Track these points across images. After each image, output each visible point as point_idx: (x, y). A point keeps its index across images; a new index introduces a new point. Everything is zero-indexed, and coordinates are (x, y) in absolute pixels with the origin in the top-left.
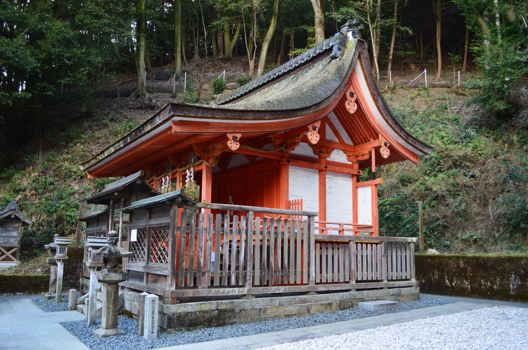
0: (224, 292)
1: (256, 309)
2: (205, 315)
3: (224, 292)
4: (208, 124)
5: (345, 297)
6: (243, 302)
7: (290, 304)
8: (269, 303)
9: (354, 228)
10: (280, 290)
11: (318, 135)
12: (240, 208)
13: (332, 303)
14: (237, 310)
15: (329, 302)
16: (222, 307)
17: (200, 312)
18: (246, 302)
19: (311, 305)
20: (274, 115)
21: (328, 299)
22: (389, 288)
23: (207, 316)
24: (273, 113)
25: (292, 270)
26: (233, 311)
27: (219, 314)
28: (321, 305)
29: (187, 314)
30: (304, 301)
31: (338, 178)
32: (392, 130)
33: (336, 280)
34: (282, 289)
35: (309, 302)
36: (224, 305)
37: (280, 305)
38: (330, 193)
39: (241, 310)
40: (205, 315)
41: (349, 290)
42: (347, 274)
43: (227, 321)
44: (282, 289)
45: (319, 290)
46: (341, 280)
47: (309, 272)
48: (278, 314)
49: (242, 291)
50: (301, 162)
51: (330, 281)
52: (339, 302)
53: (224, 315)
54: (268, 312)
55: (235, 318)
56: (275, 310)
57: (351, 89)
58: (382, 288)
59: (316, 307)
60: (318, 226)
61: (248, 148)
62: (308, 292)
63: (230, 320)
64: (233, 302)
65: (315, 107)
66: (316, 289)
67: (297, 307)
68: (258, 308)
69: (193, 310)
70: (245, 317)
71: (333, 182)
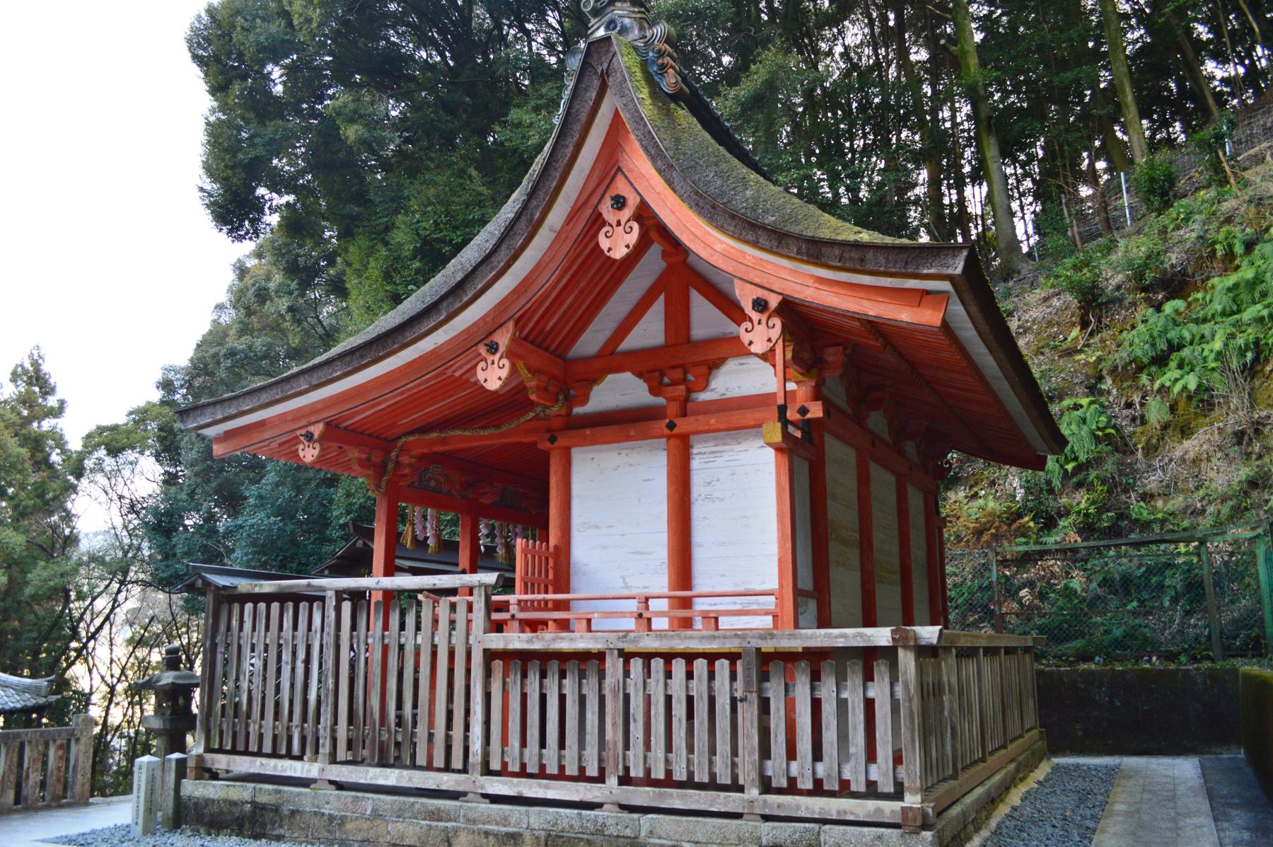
0: (275, 768)
1: (323, 814)
2: (234, 809)
3: (275, 768)
4: (262, 424)
5: (564, 823)
6: (299, 794)
7: (400, 814)
8: (351, 806)
9: (672, 607)
10: (387, 778)
11: (505, 362)
12: (309, 585)
13: (520, 835)
14: (285, 810)
15: (510, 830)
16: (262, 799)
17: (225, 801)
18: (305, 794)
19: (456, 830)
20: (351, 361)
21: (505, 821)
22: (766, 818)
23: (236, 811)
24: (348, 359)
25: (421, 731)
26: (276, 809)
27: (253, 812)
28: (487, 834)
29: (209, 802)
30: (435, 815)
31: (737, 447)
32: (483, 297)
33: (659, 774)
34: (390, 777)
35: (449, 820)
36: (266, 794)
37: (376, 815)
38: (708, 498)
39: (293, 813)
40: (234, 809)
41: (598, 806)
42: (591, 753)
43: (268, 830)
44: (390, 777)
45: (490, 791)
46: (702, 776)
47: (466, 738)
48: (371, 835)
49: (309, 771)
50: (588, 432)
51: (680, 774)
52: (543, 833)
53: (262, 815)
54: (349, 826)
55: (281, 826)
56: (365, 826)
57: (621, 187)
58: (738, 816)
59: (470, 837)
60: (666, 608)
61: (458, 432)
62: (464, 794)
63: (273, 829)
64: (280, 791)
65: (451, 299)
66: (482, 787)
67: (418, 828)
68: (327, 812)
69: (216, 797)
70: (302, 829)
71: (720, 461)
